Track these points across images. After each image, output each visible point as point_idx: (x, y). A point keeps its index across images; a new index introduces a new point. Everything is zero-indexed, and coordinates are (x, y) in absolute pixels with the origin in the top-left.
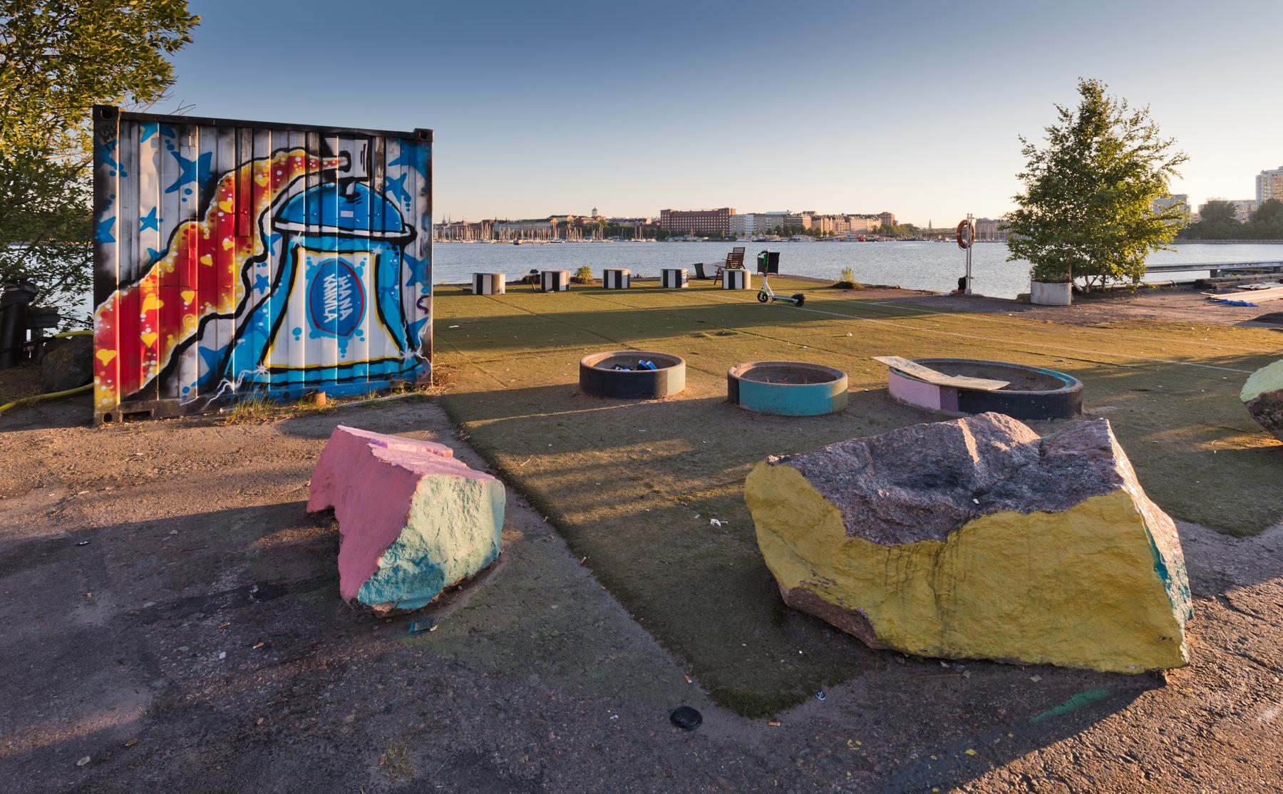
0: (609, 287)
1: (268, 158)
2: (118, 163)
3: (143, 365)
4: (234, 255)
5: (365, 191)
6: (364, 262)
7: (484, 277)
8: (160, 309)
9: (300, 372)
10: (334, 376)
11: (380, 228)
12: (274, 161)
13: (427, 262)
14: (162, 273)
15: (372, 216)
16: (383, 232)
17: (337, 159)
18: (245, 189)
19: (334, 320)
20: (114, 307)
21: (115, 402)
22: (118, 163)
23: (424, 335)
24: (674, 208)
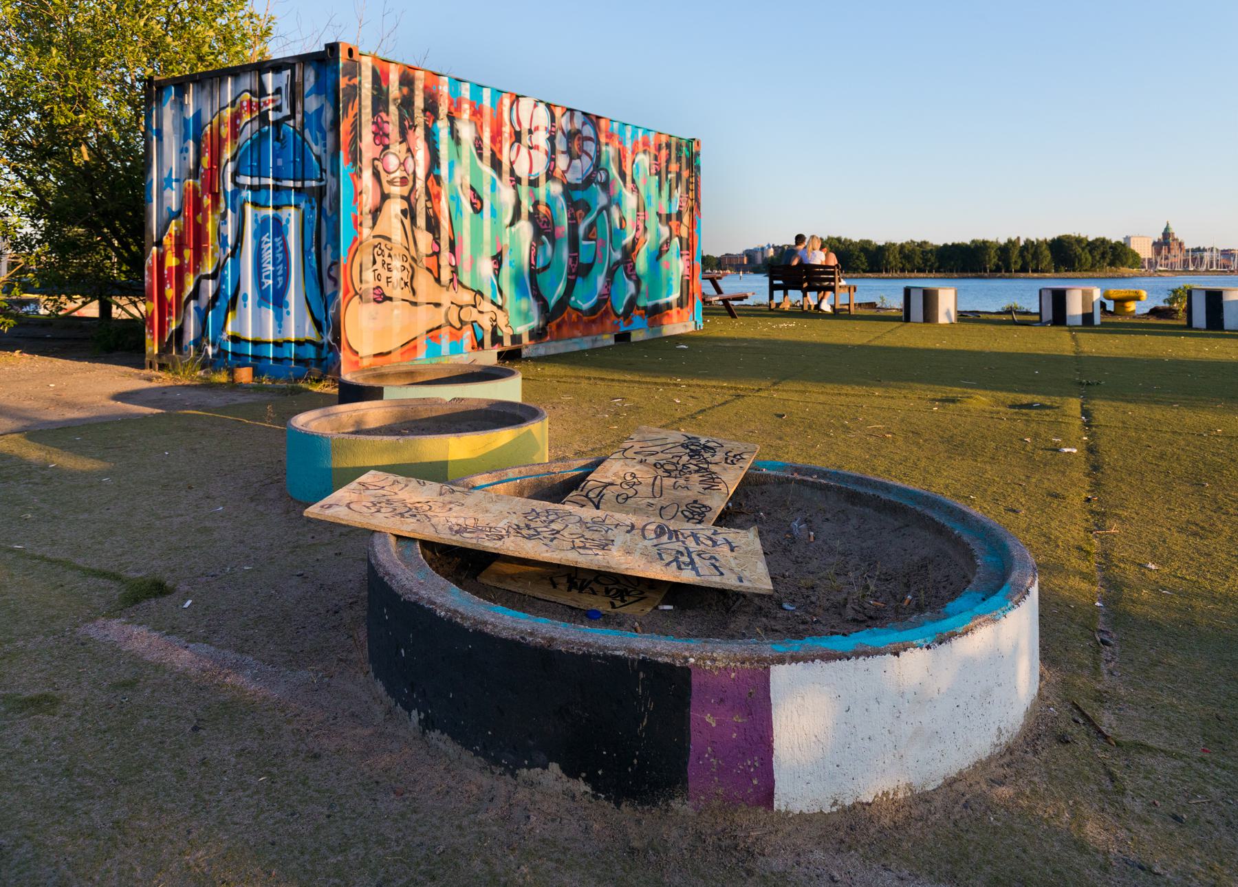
0: (1195, 325)
1: (227, 106)
2: (154, 128)
3: (167, 319)
4: (210, 212)
5: (289, 132)
6: (291, 216)
7: (913, 291)
8: (176, 267)
9: (289, 344)
10: (248, 351)
11: (257, 174)
12: (234, 109)
13: (335, 217)
14: (178, 232)
15: (1168, 282)
16: (303, 180)
17: (271, 97)
18: (216, 141)
19: (269, 286)
20: (153, 263)
21: (153, 351)
22: (154, 128)
23: (334, 314)
24: (329, 42)
